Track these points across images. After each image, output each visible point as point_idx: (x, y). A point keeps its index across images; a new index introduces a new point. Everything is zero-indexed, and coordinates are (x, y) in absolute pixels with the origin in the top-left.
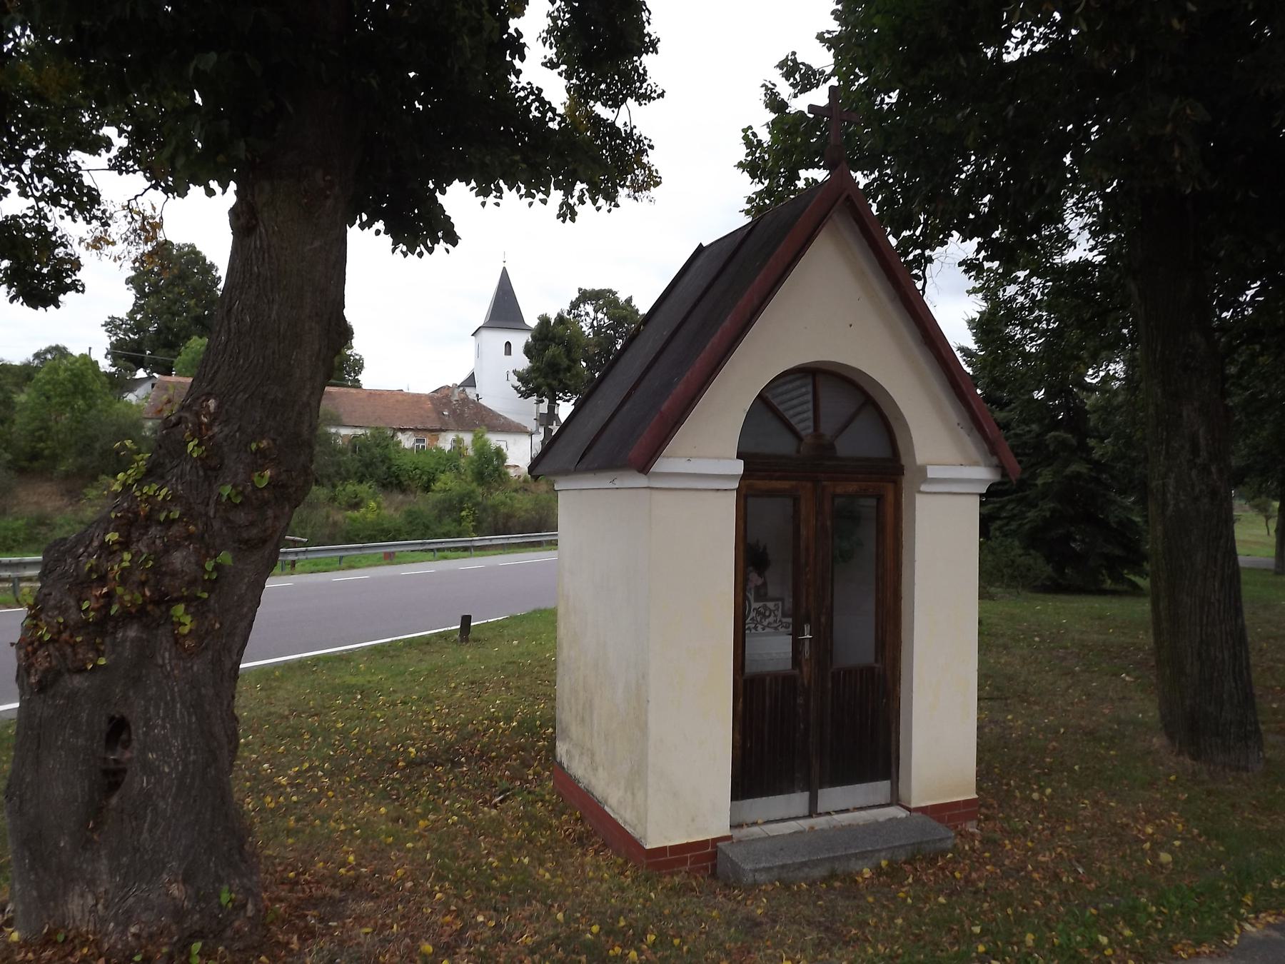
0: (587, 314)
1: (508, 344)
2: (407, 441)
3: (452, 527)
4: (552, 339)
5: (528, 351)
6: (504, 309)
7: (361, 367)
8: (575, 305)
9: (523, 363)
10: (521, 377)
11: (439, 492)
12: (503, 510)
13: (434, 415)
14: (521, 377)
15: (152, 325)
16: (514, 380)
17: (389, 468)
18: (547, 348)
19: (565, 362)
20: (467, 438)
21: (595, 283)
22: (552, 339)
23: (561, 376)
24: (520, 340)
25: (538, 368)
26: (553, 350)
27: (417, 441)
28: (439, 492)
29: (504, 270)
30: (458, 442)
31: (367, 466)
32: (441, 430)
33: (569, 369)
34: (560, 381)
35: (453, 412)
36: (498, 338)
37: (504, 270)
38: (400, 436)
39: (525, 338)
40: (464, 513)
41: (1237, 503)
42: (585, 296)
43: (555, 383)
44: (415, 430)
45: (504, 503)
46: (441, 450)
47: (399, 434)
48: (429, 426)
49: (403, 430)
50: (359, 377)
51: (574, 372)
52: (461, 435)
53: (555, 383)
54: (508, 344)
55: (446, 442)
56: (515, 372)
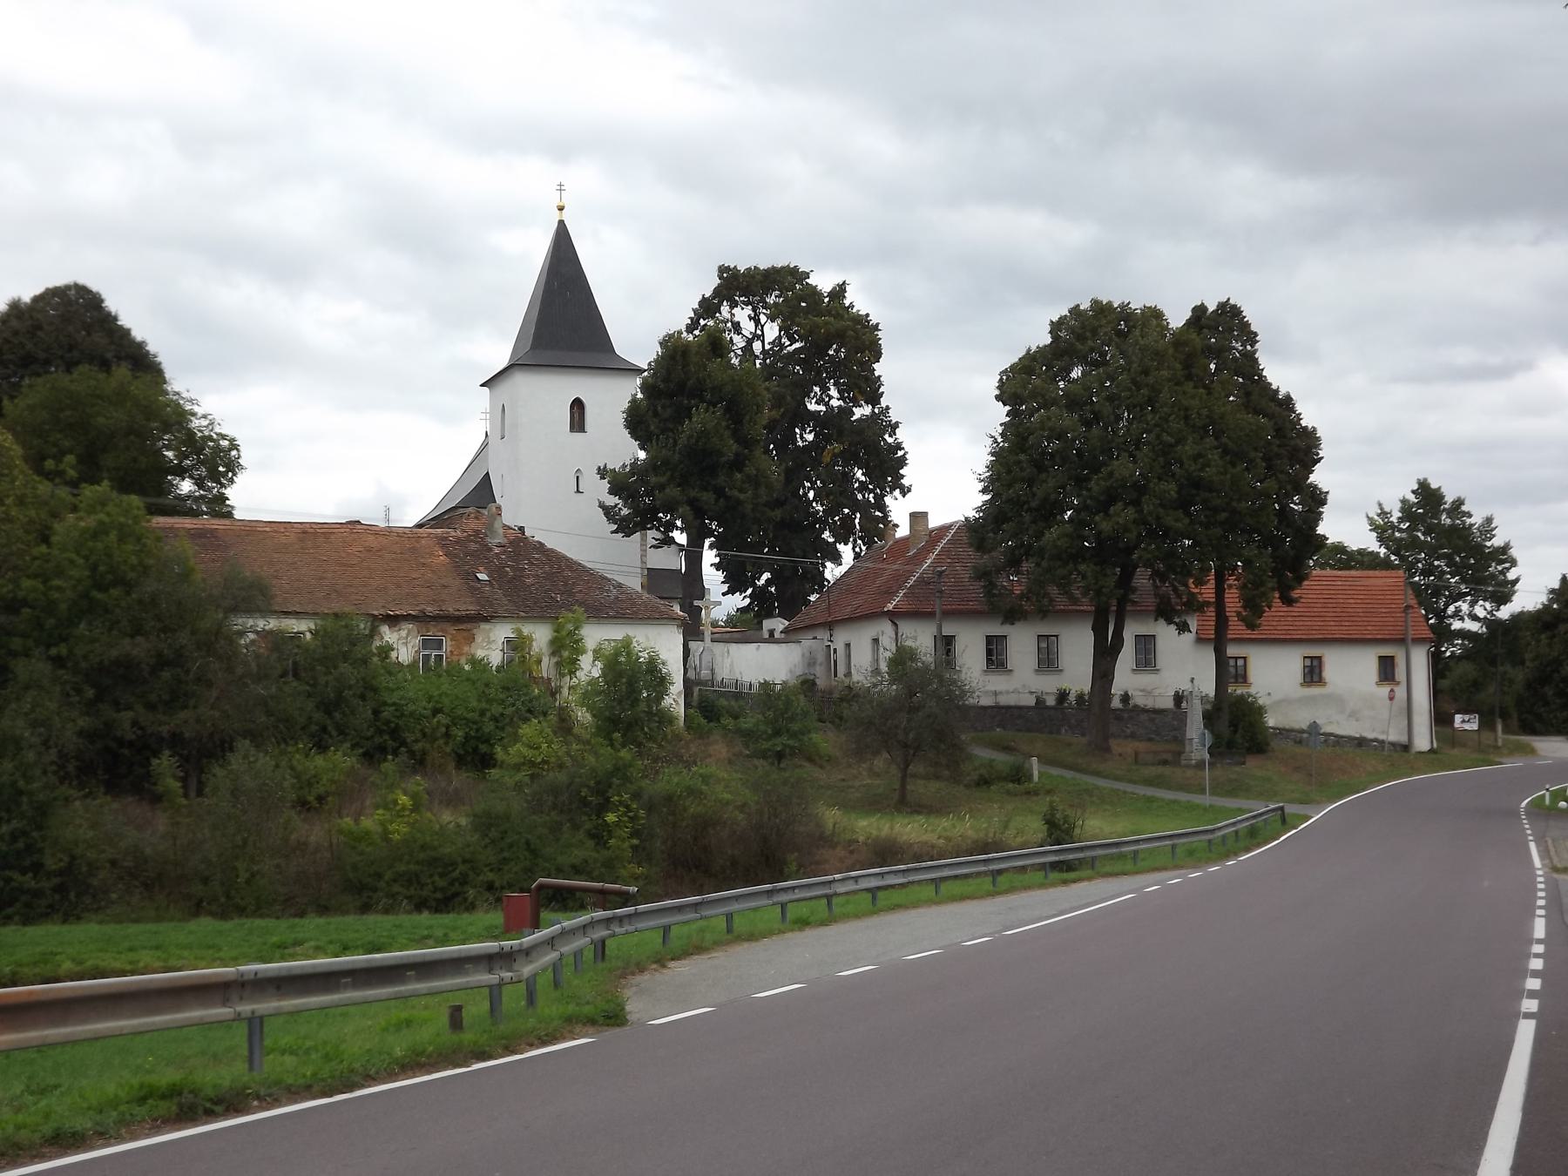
0: (737, 327)
1: (578, 406)
2: (403, 645)
3: (584, 851)
4: (698, 393)
5: (637, 422)
6: (563, 321)
7: (233, 467)
8: (707, 307)
9: (628, 452)
10: (620, 483)
11: (517, 768)
12: (694, 808)
13: (456, 583)
14: (620, 483)
15: (1292, 546)
16: (600, 490)
17: (376, 712)
18: (683, 413)
19: (731, 448)
20: (540, 635)
21: (757, 252)
22: (698, 393)
23: (721, 479)
24: (610, 400)
25: (666, 462)
26: (702, 419)
27: (426, 644)
28: (517, 768)
29: (561, 223)
30: (517, 645)
31: (328, 707)
32: (486, 619)
33: (738, 464)
34: (719, 492)
35: (497, 573)
36: (551, 392)
37: (561, 223)
38: (389, 635)
39: (628, 390)
40: (611, 818)
41: (930, 659)
42: (737, 285)
43: (707, 497)
44: (421, 619)
45: (691, 791)
46: (479, 665)
47: (385, 629)
48: (450, 609)
49: (393, 620)
50: (228, 492)
51: (750, 470)
52: (527, 629)
53: (707, 497)
54: (578, 406)
55: (490, 645)
56: (602, 472)
